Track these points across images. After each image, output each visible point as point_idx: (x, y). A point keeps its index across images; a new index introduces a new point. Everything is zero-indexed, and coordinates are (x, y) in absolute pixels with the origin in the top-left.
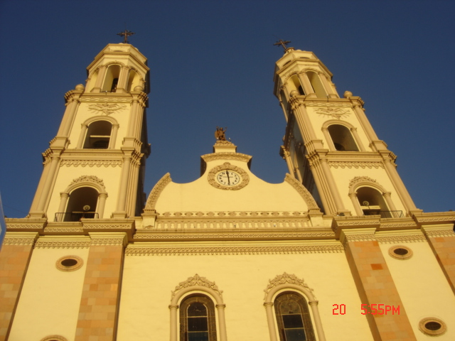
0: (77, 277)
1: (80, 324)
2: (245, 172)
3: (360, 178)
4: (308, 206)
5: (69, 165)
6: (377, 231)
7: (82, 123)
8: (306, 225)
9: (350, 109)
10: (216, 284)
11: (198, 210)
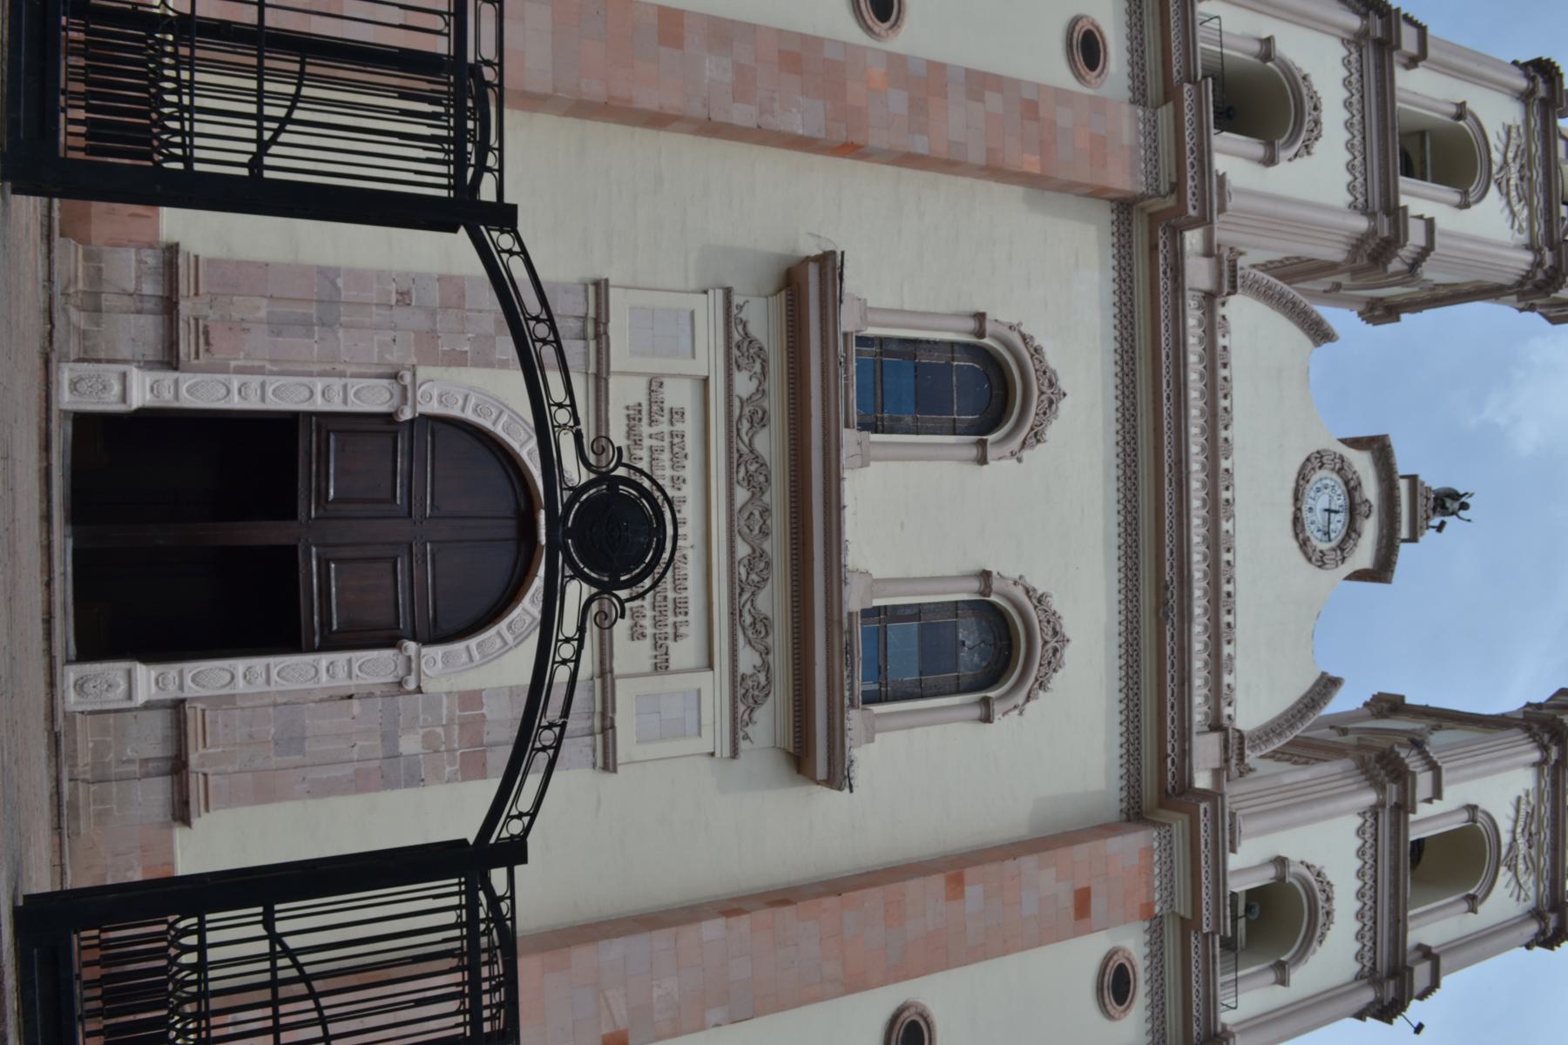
0: (1054, 70)
1: (937, 69)
2: (1343, 559)
3: (1328, 899)
4: (1253, 732)
5: (1346, 63)
6: (1182, 919)
7: (1469, 106)
8: (1198, 717)
9: (1531, 903)
10: (1039, 446)
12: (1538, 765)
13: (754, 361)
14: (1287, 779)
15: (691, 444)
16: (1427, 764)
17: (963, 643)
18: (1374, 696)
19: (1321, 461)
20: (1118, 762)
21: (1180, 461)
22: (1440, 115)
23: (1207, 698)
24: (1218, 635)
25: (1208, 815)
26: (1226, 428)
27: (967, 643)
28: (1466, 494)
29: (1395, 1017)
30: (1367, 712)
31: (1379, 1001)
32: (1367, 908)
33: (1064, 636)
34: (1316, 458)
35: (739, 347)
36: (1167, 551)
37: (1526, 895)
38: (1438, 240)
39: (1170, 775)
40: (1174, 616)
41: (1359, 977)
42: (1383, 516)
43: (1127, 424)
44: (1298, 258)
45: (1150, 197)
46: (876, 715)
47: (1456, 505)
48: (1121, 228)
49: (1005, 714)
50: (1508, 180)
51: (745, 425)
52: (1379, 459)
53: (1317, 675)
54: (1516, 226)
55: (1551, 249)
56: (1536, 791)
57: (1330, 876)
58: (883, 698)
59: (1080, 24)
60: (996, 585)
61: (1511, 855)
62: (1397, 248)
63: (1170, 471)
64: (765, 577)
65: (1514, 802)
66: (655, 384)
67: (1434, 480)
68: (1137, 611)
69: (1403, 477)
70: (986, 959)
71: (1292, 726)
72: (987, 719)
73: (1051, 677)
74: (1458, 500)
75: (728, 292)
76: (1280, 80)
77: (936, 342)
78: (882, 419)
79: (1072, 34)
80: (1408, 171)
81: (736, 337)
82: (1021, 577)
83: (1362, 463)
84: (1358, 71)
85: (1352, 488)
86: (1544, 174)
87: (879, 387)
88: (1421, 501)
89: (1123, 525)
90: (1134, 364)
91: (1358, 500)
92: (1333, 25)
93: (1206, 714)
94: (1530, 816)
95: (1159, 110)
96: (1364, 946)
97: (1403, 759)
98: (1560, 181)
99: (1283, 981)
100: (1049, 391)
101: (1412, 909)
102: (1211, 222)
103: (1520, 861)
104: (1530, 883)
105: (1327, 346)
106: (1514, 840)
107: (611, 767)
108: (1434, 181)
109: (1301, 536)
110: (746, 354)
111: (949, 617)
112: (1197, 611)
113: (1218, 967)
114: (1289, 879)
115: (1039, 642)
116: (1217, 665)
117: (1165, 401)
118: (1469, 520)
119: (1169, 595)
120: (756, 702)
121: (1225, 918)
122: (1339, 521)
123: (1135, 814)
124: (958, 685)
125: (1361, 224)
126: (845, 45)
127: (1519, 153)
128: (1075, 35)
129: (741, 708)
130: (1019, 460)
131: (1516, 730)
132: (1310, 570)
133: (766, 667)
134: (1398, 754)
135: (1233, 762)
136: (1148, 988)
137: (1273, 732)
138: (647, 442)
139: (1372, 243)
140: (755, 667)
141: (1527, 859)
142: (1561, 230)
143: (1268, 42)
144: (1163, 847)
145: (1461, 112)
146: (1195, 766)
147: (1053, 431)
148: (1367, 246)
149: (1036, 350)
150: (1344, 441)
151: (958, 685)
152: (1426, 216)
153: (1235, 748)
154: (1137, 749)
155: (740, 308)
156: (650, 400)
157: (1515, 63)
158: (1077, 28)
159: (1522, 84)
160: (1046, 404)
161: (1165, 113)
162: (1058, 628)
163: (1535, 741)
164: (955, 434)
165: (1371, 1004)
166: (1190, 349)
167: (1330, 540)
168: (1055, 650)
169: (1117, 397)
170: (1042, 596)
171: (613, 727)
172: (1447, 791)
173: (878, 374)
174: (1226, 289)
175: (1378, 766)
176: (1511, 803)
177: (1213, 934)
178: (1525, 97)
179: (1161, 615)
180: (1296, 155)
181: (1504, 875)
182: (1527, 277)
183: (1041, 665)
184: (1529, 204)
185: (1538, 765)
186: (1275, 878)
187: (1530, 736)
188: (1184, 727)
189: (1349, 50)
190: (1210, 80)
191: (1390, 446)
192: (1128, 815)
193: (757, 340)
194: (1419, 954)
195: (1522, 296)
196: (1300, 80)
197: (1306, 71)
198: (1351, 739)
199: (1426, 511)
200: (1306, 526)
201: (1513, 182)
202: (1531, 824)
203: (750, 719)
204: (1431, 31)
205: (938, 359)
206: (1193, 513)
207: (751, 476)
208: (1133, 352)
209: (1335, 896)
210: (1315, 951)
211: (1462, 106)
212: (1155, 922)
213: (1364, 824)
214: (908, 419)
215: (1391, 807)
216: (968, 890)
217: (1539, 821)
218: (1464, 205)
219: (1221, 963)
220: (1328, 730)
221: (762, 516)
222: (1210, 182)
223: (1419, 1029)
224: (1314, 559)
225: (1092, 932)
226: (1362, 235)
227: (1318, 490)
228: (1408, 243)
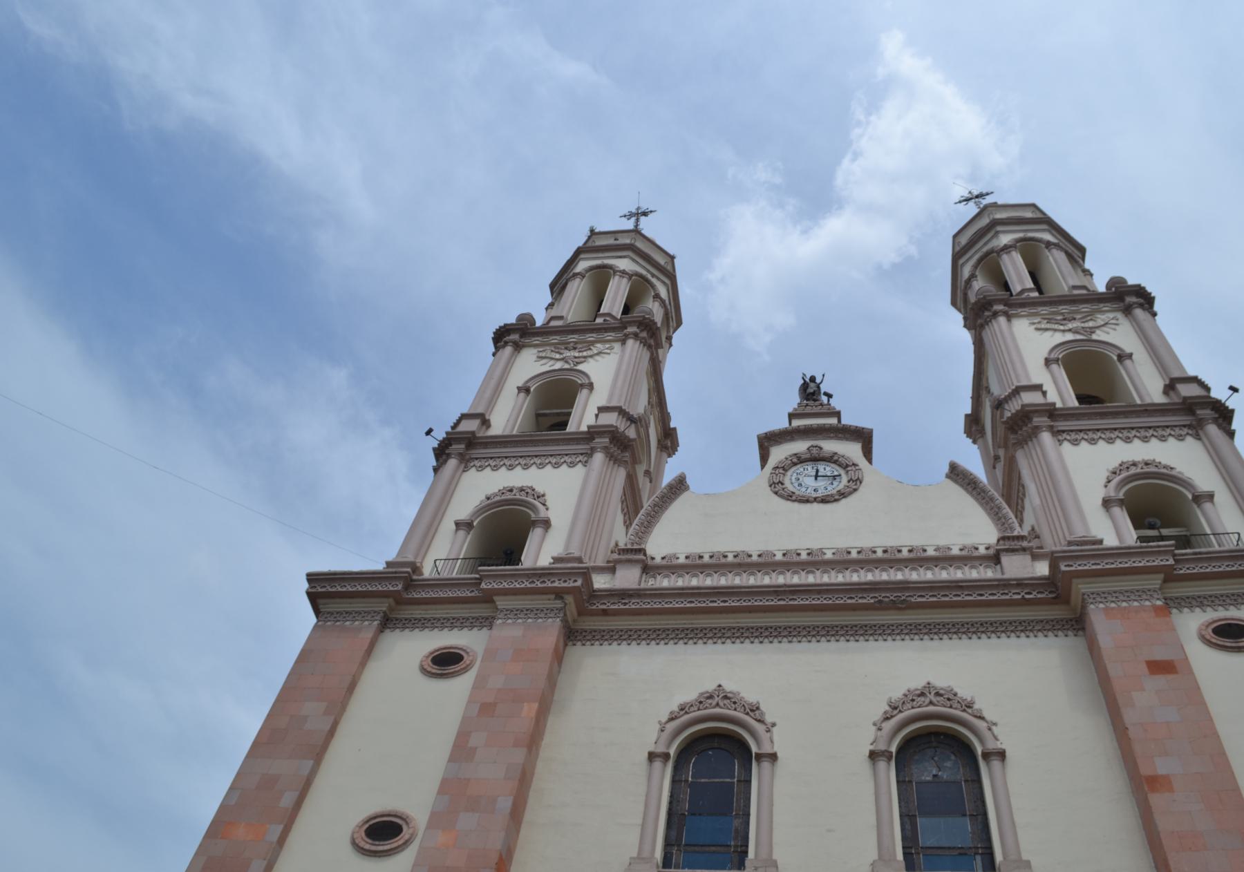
0: (460, 687)
1: (446, 786)
2: (854, 465)
3: (1134, 464)
4: (999, 530)
5: (481, 469)
6: (1165, 581)
7: (520, 385)
8: (989, 574)
9: (1119, 315)
10: (762, 707)
11: (738, 548)
12: (1009, 317)
14: (1037, 501)
16: (1015, 396)
17: (935, 776)
18: (967, 437)
19: (778, 484)
20: (1032, 639)
21: (776, 592)
22: (527, 402)
23: (972, 567)
24: (919, 559)
25: (1070, 563)
26: (750, 556)
27: (934, 772)
28: (803, 378)
29: (1227, 407)
30: (980, 441)
31: (1215, 421)
32: (1138, 434)
33: (925, 687)
34: (775, 487)
36: (849, 601)
37: (1113, 319)
38: (614, 403)
39: (1039, 596)
40: (904, 596)
41: (1197, 437)
42: (820, 436)
43: (745, 635)
44: (622, 502)
45: (565, 615)
46: (1004, 858)
47: (812, 385)
48: (588, 638)
49: (996, 738)
50: (575, 357)
52: (777, 441)
53: (948, 481)
54: (608, 351)
55: (626, 328)
56: (1029, 318)
57: (1114, 464)
58: (988, 851)
59: (426, 667)
60: (881, 746)
61: (1082, 332)
62: (618, 432)
63: (784, 600)
65: (1039, 333)
67: (793, 400)
68: (901, 625)
69: (790, 424)
70: (1224, 754)
71: (992, 499)
72: (1002, 755)
74: (808, 384)
76: (486, 516)
77: (671, 796)
78: (736, 846)
79: (433, 674)
80: (564, 425)
82: (875, 724)
83: (779, 453)
84: (488, 461)
85: (798, 460)
86: (573, 334)
87: (707, 849)
88: (808, 410)
89: (828, 638)
90: (697, 629)
91: (808, 456)
92: (453, 477)
93: (986, 567)
94: (1049, 321)
95: (499, 607)
96: (1170, 435)
97: (1012, 414)
98: (579, 323)
99: (1210, 497)
100: (717, 699)
101: (1135, 401)
102: (587, 568)
103: (1086, 325)
104: (1103, 317)
105: (689, 481)
106: (1070, 330)
108: (572, 407)
109: (837, 497)
111: (912, 789)
112: (900, 576)
113: (1203, 550)
114: (1121, 495)
115: (931, 708)
116: (944, 559)
117: (727, 604)
118: (824, 375)
119: (887, 599)
121: (1159, 546)
122: (825, 469)
123: (1077, 623)
124: (973, 781)
125: (599, 457)
127: (557, 350)
128: (434, 671)
130: (774, 725)
131: (984, 334)
132: (863, 489)
134: (1008, 418)
135: (1025, 544)
136: (1232, 607)
137: (997, 514)
139: (614, 449)
141: (1084, 320)
142: (613, 321)
143: (458, 524)
144: (1103, 600)
145: (524, 390)
146: (1030, 575)
147: (750, 697)
148: (616, 454)
149: (682, 710)
150: (763, 467)
151: (973, 781)
152: (597, 412)
153: (1013, 543)
154: (1020, 623)
157: (494, 355)
158: (429, 669)
159: (508, 350)
160: (726, 702)
161: (501, 602)
162: (918, 692)
163: (990, 321)
164: (750, 781)
165: (1220, 426)
166: (686, 584)
167: (840, 475)
168: (938, 694)
169: (723, 643)
170: (890, 706)
172: (1035, 380)
173: (696, 849)
174: (641, 557)
175: (1020, 432)
176: (1041, 334)
177: (1174, 555)
178: (518, 347)
179: (904, 606)
182: (644, 343)
183: (951, 707)
184: (593, 343)
185: (1009, 317)
186: (1121, 507)
187: (988, 324)
188: (998, 585)
189: (472, 467)
190: (480, 568)
191: (766, 434)
192: (1079, 629)
194: (1171, 393)
195: (659, 345)
196: (489, 501)
197: (483, 497)
198: (1001, 452)
199: (816, 406)
200: (829, 493)
201: (577, 355)
202: (1056, 320)
204: (465, 411)
205: (686, 794)
206: (818, 581)
208: (687, 629)
209: (1130, 459)
210: (1180, 473)
211: (519, 389)
212: (1171, 604)
213: (1069, 441)
214: (736, 823)
215: (1052, 421)
218: (591, 386)
219: (1200, 547)
220: (997, 470)
222: (557, 569)
223: (429, 432)
224: (854, 487)
225: (1187, 658)
226: (607, 457)
227: (800, 485)
228: (615, 424)
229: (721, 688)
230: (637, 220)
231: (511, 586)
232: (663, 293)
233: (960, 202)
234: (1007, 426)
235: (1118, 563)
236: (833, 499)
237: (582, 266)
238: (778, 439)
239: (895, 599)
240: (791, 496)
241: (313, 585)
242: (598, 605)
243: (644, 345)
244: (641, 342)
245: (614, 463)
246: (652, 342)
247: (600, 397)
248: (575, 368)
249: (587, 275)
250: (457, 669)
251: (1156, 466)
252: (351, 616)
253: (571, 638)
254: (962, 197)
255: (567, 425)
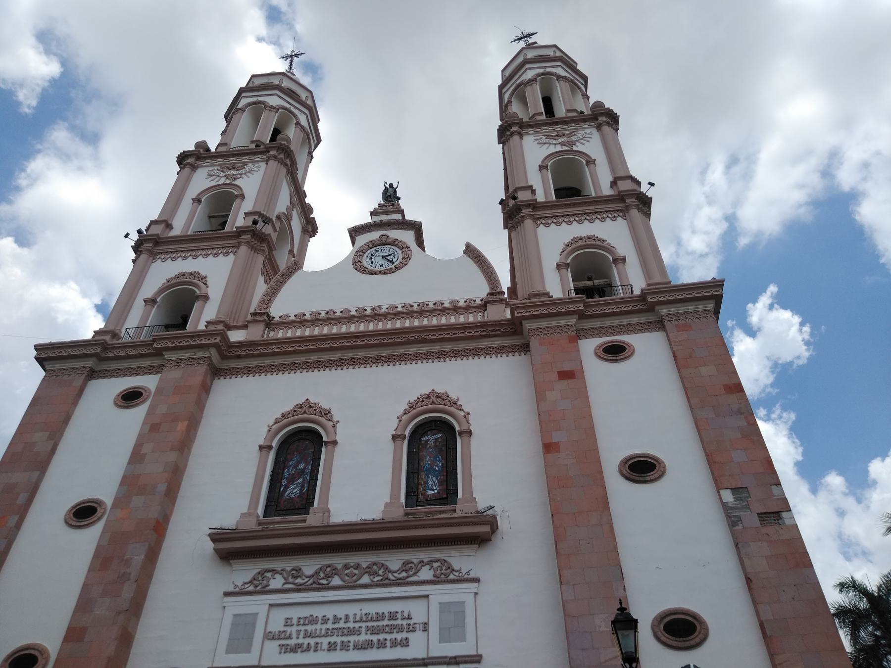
0: (138, 413)
3: (581, 239)
4: (490, 288)
9: (594, 131)
11: (328, 308)
13: (265, 577)
15: (305, 612)
28: (384, 185)
31: (637, 206)
35: (256, 587)
41: (624, 217)
48: (228, 374)
50: (234, 175)
51: (299, 581)
54: (256, 169)
57: (568, 239)
64: (381, 565)
66: (270, 636)
72: (470, 433)
73: (451, 398)
74: (388, 189)
75: (227, 594)
81: (251, 588)
82: (398, 418)
83: (362, 240)
86: (245, 156)
94: (548, 137)
100: (305, 408)
104: (582, 132)
107: (477, 658)
109: (394, 270)
110: (261, 582)
115: (433, 406)
118: (398, 182)
119: (413, 338)
120: (449, 568)
125: (243, 249)
126: (103, 533)
127: (221, 170)
129: (452, 577)
132: (411, 263)
133: (430, 563)
138: (300, 641)
140: (430, 569)
143: (145, 301)
145: (197, 200)
147: (325, 405)
155: (236, 586)
156: (278, 639)
161: (169, 356)
163: (509, 139)
171: (455, 658)
178: (194, 168)
180: (206, 284)
181: (577, 146)
183: (444, 404)
184: (246, 164)
193: (254, 576)
194: (615, 187)
196: (169, 283)
197: (165, 281)
201: (235, 172)
202: (552, 136)
203: (458, 571)
207: (326, 576)
216: (555, 440)
217: (550, 132)
218: (243, 197)
221: (349, 569)
223: (127, 236)
224: (405, 263)
227: (372, 262)
229: (308, 401)
230: (291, 62)
231: (166, 346)
232: (303, 120)
233: (515, 41)
234: (507, 215)
235: (694, 294)
236: (391, 271)
237: (243, 102)
238: (361, 231)
239: (418, 338)
240: (365, 271)
241: (39, 353)
242: (233, 352)
243: (281, 164)
244: (279, 162)
245: (255, 252)
246: (288, 161)
247: (247, 205)
248: (233, 183)
249: (246, 110)
250: (137, 403)
251: (594, 240)
252: (67, 371)
253: (217, 374)
254: (516, 37)
255: (257, 224)
